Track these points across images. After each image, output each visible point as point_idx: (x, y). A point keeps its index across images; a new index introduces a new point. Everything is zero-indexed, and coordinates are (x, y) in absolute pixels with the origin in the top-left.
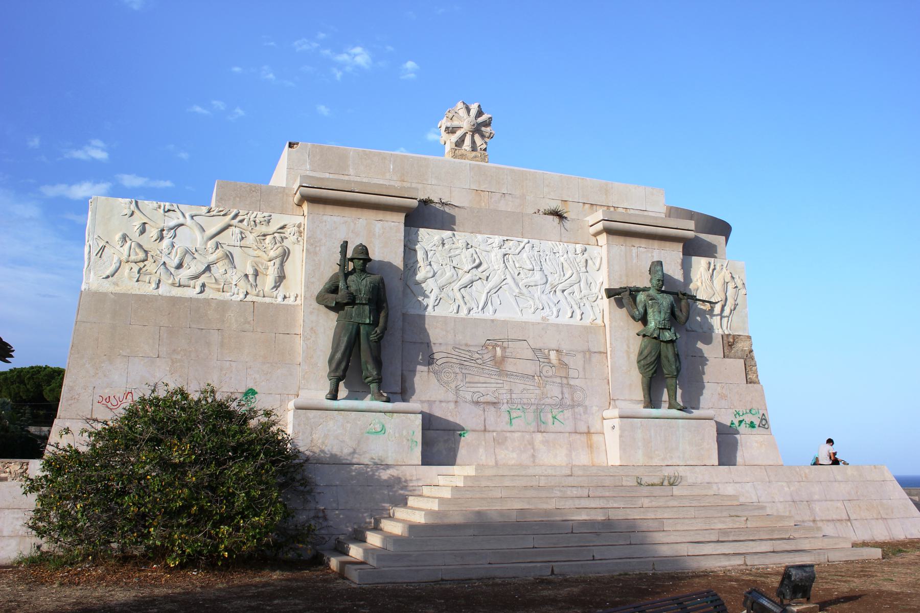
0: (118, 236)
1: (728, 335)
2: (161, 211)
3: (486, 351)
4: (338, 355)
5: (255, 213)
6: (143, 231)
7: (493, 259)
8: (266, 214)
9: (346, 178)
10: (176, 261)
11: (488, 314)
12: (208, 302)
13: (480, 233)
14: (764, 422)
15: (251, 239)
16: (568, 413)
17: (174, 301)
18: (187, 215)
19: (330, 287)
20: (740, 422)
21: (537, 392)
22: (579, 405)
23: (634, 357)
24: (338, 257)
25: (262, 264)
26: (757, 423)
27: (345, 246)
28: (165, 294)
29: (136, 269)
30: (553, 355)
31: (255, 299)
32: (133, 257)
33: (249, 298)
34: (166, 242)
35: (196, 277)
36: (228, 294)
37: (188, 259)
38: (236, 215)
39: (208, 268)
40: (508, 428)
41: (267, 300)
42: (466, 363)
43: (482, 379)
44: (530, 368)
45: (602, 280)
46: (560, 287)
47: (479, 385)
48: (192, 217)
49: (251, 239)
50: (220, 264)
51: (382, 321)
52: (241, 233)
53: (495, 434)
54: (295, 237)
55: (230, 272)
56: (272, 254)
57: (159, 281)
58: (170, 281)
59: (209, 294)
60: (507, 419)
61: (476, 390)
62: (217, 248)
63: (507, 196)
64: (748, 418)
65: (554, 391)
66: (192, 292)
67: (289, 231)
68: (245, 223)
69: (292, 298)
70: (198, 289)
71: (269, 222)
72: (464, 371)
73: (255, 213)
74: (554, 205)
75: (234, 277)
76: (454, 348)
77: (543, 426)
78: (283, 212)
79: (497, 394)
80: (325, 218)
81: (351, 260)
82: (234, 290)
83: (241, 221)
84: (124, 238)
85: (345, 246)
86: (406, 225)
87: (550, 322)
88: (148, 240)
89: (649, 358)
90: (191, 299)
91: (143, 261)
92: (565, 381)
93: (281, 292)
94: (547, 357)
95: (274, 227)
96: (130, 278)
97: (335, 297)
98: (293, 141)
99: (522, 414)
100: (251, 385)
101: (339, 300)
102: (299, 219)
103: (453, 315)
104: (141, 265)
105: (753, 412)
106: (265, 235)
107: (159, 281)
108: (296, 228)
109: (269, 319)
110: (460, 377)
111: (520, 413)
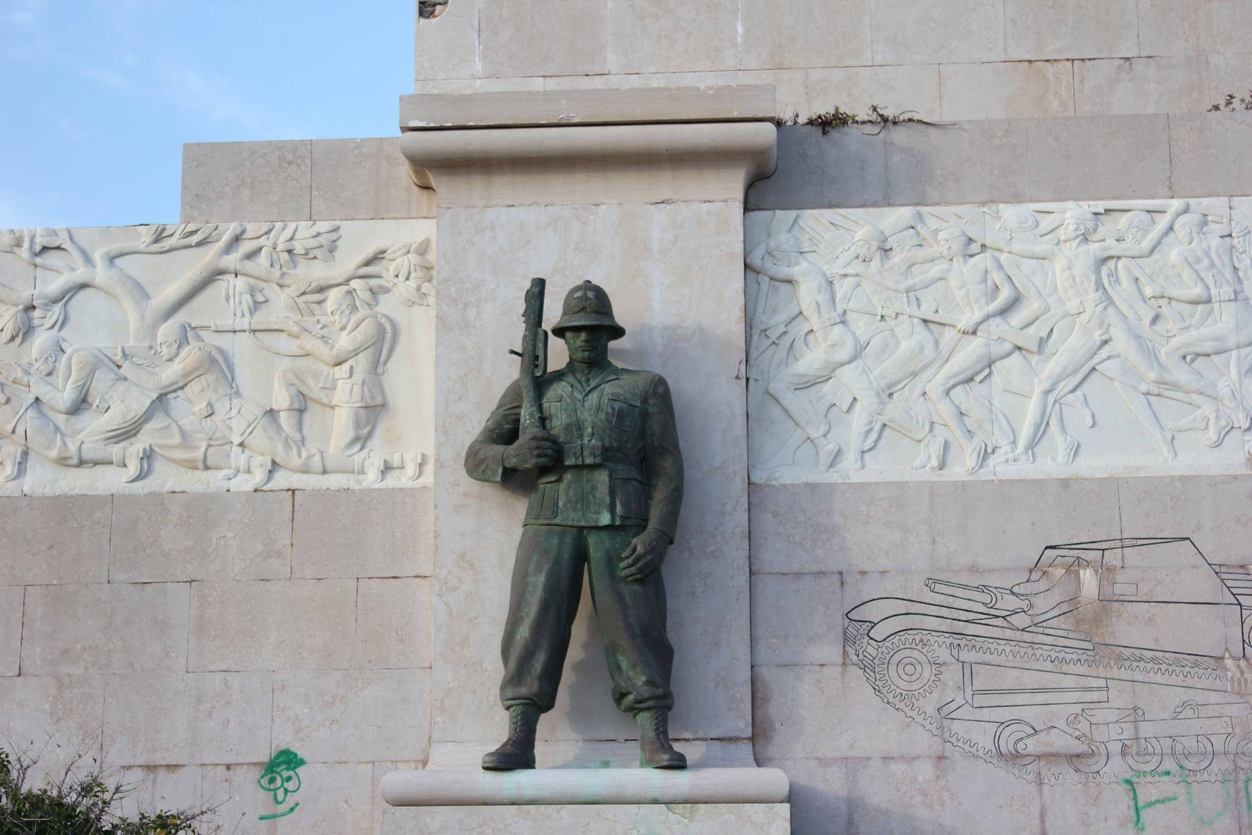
3: (1043, 585)
4: (524, 632)
11: (1052, 463)
13: (1016, 198)
21: (1234, 710)
24: (517, 334)
27: (537, 292)
33: (282, 480)
34: (41, 340)
35: (127, 433)
42: (972, 629)
43: (1030, 680)
47: (1020, 699)
59: (167, 478)
69: (411, 469)
72: (965, 656)
76: (931, 583)
79: (1083, 727)
81: (559, 332)
85: (537, 292)
93: (373, 457)
95: (347, 261)
100: (285, 740)
109: (324, 531)
110: (952, 675)
111: (1169, 786)
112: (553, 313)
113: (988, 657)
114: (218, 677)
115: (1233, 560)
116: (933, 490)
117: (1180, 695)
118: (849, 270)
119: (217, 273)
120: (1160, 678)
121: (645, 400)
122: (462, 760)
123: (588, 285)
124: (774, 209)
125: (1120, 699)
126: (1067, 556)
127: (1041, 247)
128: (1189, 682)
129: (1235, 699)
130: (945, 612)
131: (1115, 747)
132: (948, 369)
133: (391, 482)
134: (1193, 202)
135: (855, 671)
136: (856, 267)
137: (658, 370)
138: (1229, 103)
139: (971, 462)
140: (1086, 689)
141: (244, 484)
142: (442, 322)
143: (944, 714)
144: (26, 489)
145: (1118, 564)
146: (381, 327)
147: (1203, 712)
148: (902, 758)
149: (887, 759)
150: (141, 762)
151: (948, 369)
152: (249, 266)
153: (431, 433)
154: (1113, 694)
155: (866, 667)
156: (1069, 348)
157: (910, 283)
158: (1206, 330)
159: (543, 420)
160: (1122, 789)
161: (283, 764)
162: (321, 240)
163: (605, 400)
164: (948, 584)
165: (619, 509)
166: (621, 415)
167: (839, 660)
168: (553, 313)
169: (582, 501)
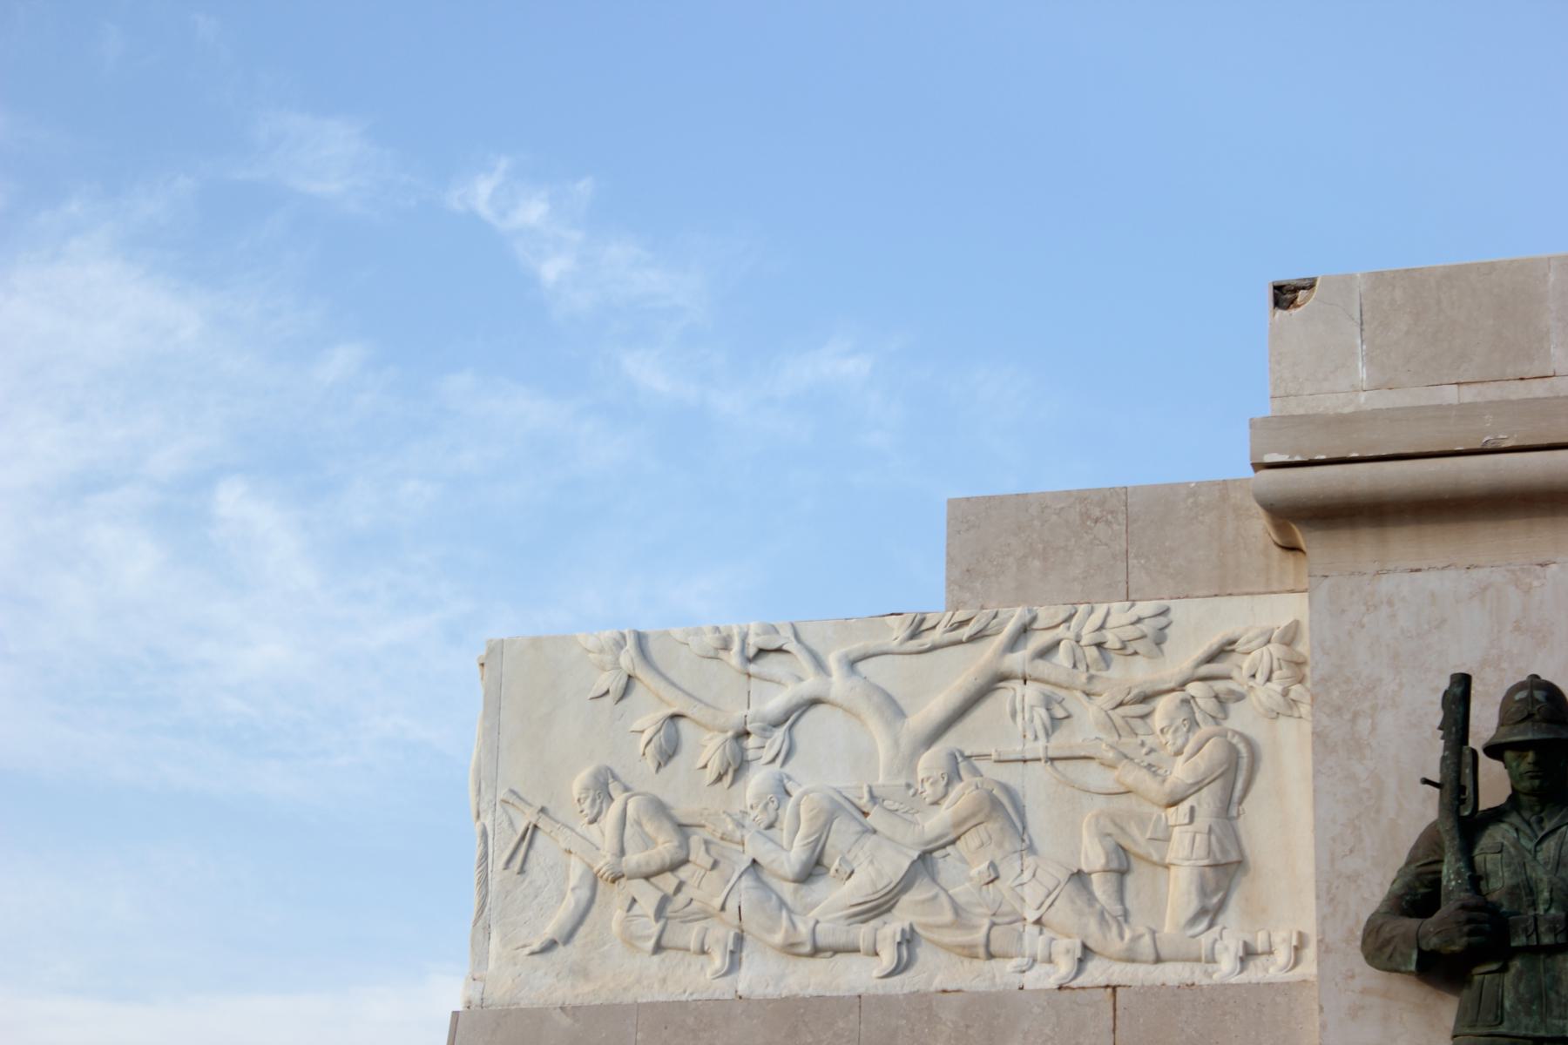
0: (579, 781)
2: (733, 657)
5: (1101, 610)
6: (668, 753)
9: (1538, 389)
10: (794, 856)
12: (924, 1004)
15: (1088, 723)
17: (794, 1013)
18: (832, 661)
19: (1409, 889)
25: (1142, 822)
27: (1460, 693)
28: (759, 992)
29: (648, 898)
31: (1119, 973)
32: (634, 859)
33: (1096, 973)
34: (758, 779)
35: (879, 907)
36: (1010, 965)
37: (841, 836)
38: (1025, 630)
39: (925, 862)
41: (1172, 973)
48: (852, 663)
49: (1088, 723)
50: (970, 841)
52: (1048, 703)
54: (1276, 686)
55: (1009, 871)
56: (1180, 772)
57: (740, 939)
58: (778, 938)
59: (936, 971)
62: (953, 776)
66: (859, 976)
67: (1246, 663)
68: (1062, 657)
69: (1282, 955)
70: (887, 958)
71: (1159, 639)
73: (1101, 610)
75: (1030, 887)
78: (1225, 586)
80: (1386, 585)
81: (1494, 751)
82: (1034, 941)
83: (1046, 652)
84: (602, 787)
85: (1460, 693)
88: (688, 786)
91: (674, 867)
93: (1228, 940)
95: (1182, 657)
96: (630, 941)
98: (1288, 276)
101: (1433, 942)
102: (1288, 609)
104: (668, 882)
106: (1145, 698)
107: (740, 939)
108: (1275, 649)
112: (1484, 723)
133: (1255, 973)
141: (1044, 978)
144: (742, 988)
146: (1233, 749)
152: (1042, 667)
162: (1144, 627)
168: (1484, 723)
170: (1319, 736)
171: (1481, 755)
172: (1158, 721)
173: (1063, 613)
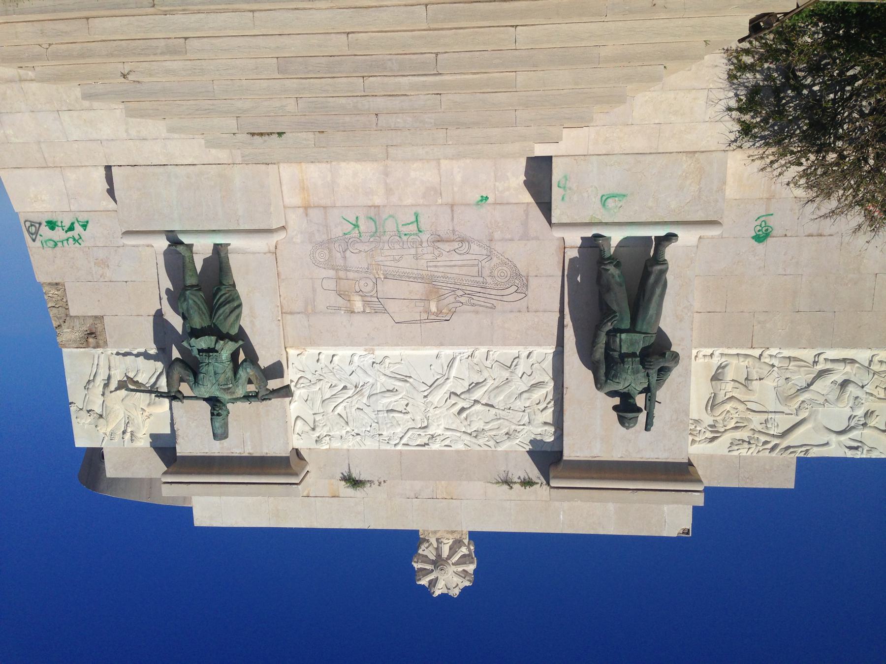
1: (97, 346)
3: (451, 306)
4: (658, 291)
7: (442, 422)
8: (736, 453)
10: (851, 388)
11: (447, 352)
13: (458, 452)
14: (33, 229)
15: (756, 420)
16: (337, 232)
20: (71, 228)
21: (380, 259)
22: (321, 244)
23: (245, 310)
24: (658, 410)
26: (45, 230)
27: (648, 426)
30: (358, 305)
33: (756, 353)
34: (860, 412)
35: (822, 374)
40: (419, 210)
42: (478, 290)
43: (456, 270)
44: (389, 288)
45: (294, 407)
46: (350, 393)
47: (460, 263)
51: (603, 339)
53: (440, 201)
59: (808, 354)
60: (422, 220)
61: (462, 257)
63: (412, 495)
64: (59, 234)
65: (356, 260)
69: (700, 355)
72: (481, 279)
74: (359, 493)
76: (493, 307)
77: (372, 215)
78: (711, 458)
79: (436, 252)
81: (639, 410)
85: (648, 426)
86: (561, 453)
87: (362, 348)
89: (228, 311)
90: (832, 346)
92: (342, 274)
93: (716, 361)
94: (366, 303)
95: (727, 438)
97: (658, 356)
99: (401, 228)
100: (760, 247)
103: (494, 349)
105: (51, 244)
109: (734, 329)
110: (486, 272)
111: (405, 230)
112: (642, 417)
113: (472, 279)
114: (788, 272)
115: (380, 315)
116: (492, 343)
117: (400, 264)
118: (522, 427)
119: (784, 435)
120: (408, 270)
121: (606, 381)
122: (686, 237)
123: (627, 428)
124: (551, 452)
125: (422, 263)
126: (443, 316)
127: (449, 433)
128: (397, 269)
129: (380, 263)
130: (488, 296)
131: (425, 244)
132: (485, 388)
133: (709, 351)
134: (393, 448)
135: (523, 274)
136: (519, 428)
137: (598, 392)
138: (380, 483)
139: (477, 353)
140: (436, 266)
141: (774, 351)
142: (687, 413)
143: (489, 257)
144: (869, 351)
145: (423, 314)
146: (712, 409)
147: (392, 258)
148: (506, 240)
149: (512, 240)
150: (824, 238)
151: (485, 388)
152: (768, 439)
153: (692, 370)
154: (425, 265)
155: (519, 275)
156: (438, 396)
157: (499, 422)
158: (389, 400)
159: (648, 375)
160: (423, 228)
161: (761, 237)
162: (736, 448)
163: (622, 383)
164: (487, 307)
165: (618, 340)
166: (615, 376)
167: (530, 279)
168: (642, 417)
169: (632, 343)
170: (687, 414)
171: (643, 408)
172: (734, 421)
173: (760, 454)
